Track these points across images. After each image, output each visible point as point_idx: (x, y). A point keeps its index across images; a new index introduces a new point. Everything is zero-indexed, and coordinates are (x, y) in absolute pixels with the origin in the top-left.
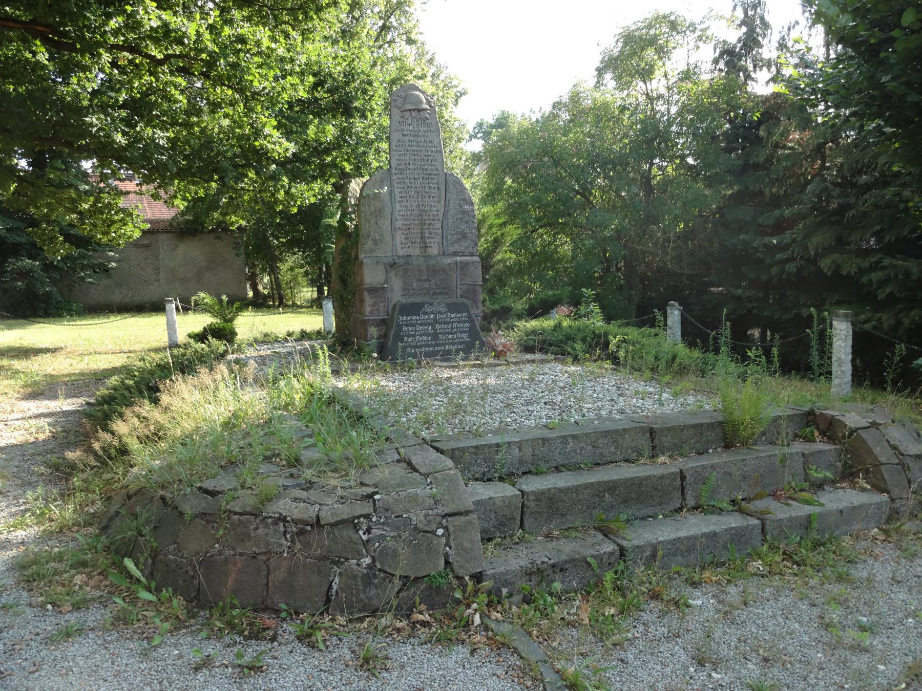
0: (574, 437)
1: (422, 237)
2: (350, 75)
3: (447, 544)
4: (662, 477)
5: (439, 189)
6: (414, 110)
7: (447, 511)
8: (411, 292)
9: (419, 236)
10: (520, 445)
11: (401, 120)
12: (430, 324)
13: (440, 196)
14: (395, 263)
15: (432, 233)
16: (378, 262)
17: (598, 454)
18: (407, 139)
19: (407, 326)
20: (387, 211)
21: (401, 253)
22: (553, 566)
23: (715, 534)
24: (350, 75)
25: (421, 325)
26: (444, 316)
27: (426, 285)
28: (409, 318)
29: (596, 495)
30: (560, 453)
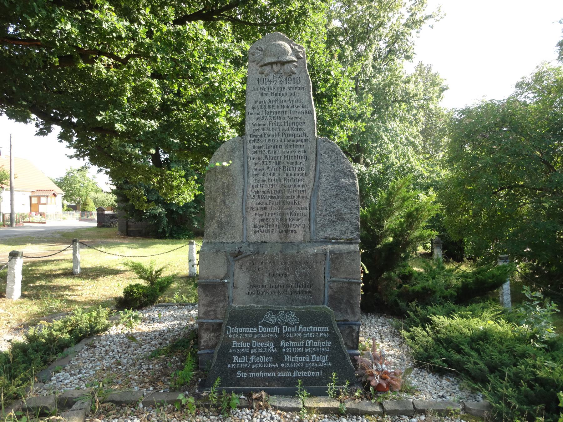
5: (306, 158)
6: (276, 63)
8: (261, 289)
9: (279, 217)
11: (260, 76)
12: (269, 339)
13: (308, 168)
14: (240, 253)
15: (296, 214)
16: (217, 251)
18: (266, 98)
20: (238, 188)
21: (253, 238)
26: (294, 330)
27: (282, 281)
28: (242, 330)
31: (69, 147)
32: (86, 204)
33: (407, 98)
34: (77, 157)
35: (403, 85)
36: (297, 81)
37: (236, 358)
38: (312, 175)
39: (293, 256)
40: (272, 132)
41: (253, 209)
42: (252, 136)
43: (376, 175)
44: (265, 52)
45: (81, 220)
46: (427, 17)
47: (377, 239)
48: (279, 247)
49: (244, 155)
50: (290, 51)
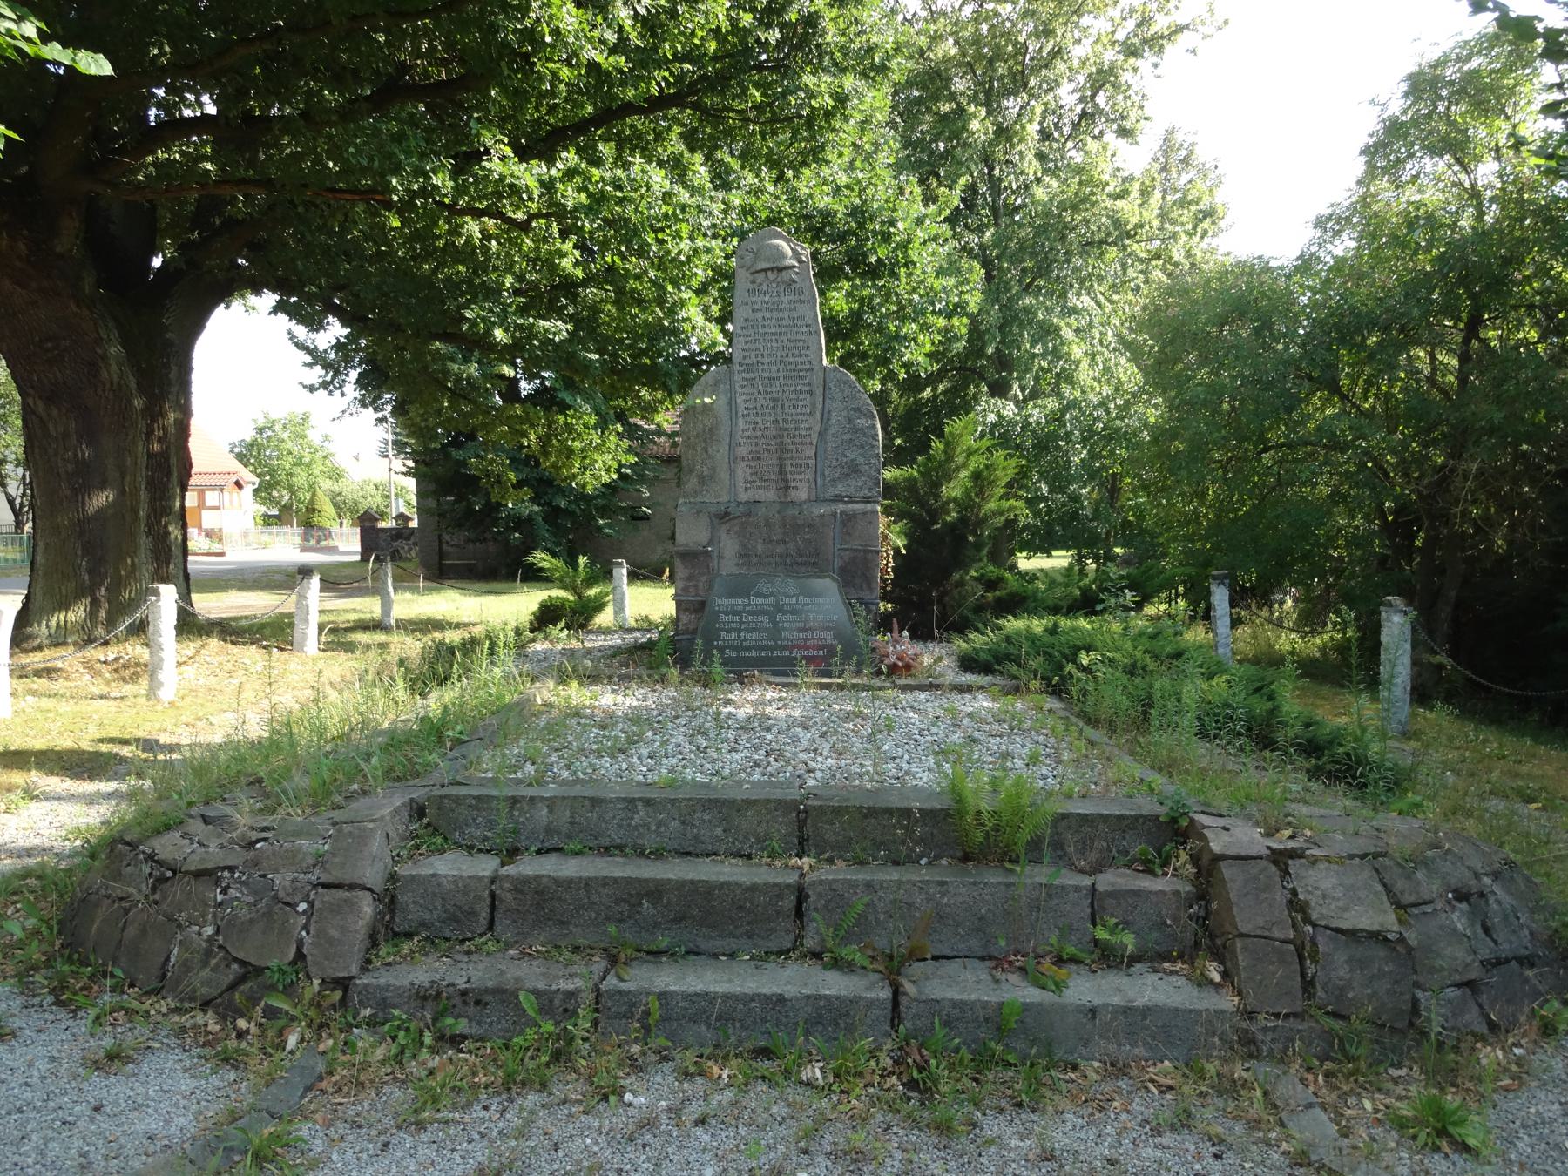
0: (648, 802)
1: (781, 472)
2: (860, 213)
3: (305, 927)
4: (753, 888)
5: (812, 393)
6: (772, 269)
7: (324, 878)
10: (551, 803)
11: (751, 286)
13: (814, 405)
14: (727, 514)
16: (698, 512)
17: (689, 836)
18: (759, 315)
19: (726, 614)
20: (723, 431)
21: (744, 497)
22: (464, 993)
23: (781, 999)
24: (860, 213)
25: (751, 613)
26: (793, 601)
27: (780, 549)
29: (625, 901)
30: (620, 826)
31: (310, 365)
32: (314, 510)
33: (1121, 233)
34: (326, 388)
35: (1109, 203)
36: (799, 292)
37: (723, 634)
38: (818, 415)
39: (794, 517)
40: (766, 360)
41: (743, 459)
42: (741, 364)
43: (1039, 424)
44: (757, 255)
45: (304, 549)
46: (1179, 29)
47: (934, 515)
48: (777, 507)
49: (732, 390)
50: (790, 253)
